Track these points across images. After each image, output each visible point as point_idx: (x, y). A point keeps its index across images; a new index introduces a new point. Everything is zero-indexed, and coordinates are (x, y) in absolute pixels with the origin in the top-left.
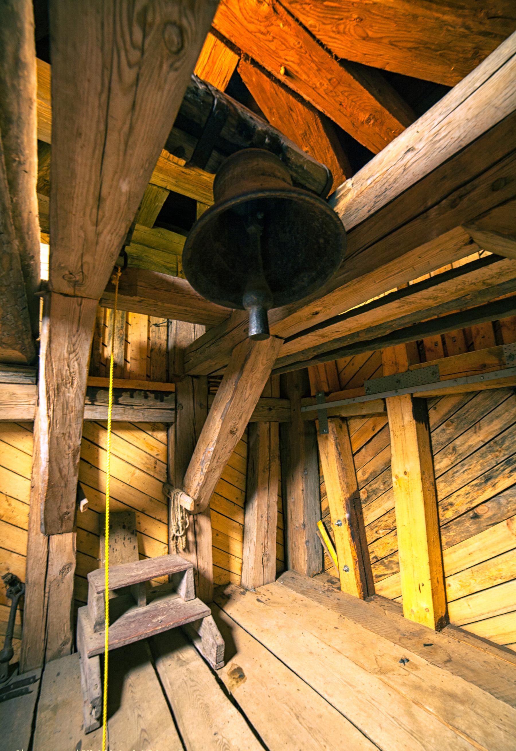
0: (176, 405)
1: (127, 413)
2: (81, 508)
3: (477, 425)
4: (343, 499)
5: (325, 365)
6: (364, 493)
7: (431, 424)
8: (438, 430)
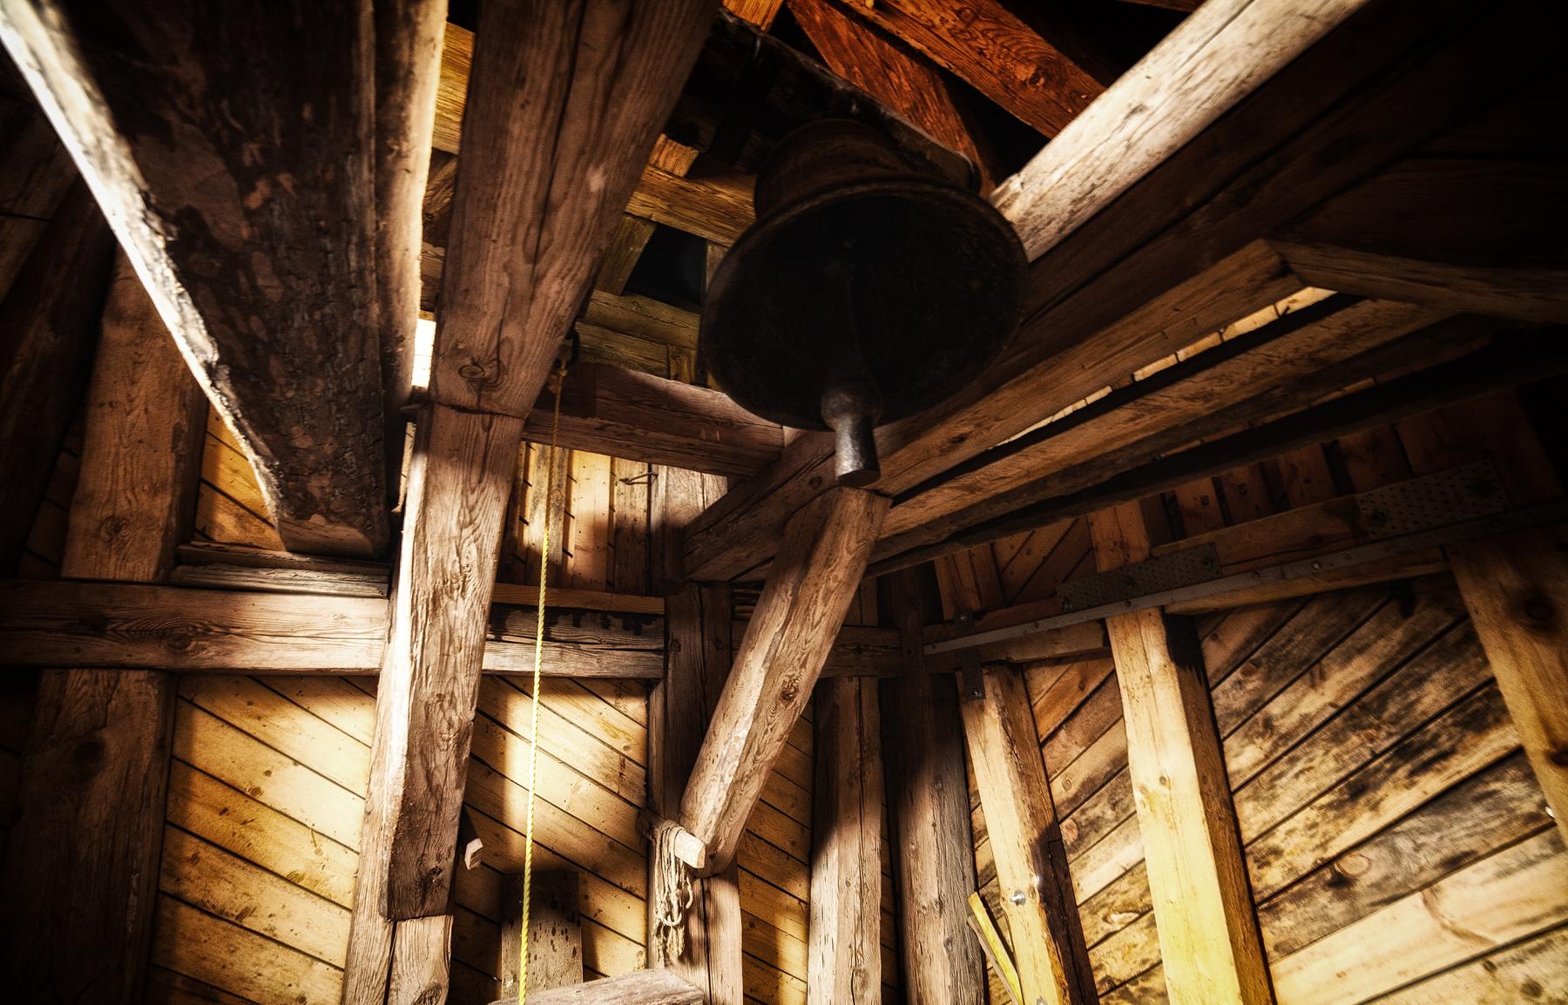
0: (666, 643)
1: (567, 658)
2: (468, 860)
3: (1316, 670)
4: (1024, 842)
5: (971, 555)
6: (1069, 828)
7: (1210, 670)
8: (1227, 684)
